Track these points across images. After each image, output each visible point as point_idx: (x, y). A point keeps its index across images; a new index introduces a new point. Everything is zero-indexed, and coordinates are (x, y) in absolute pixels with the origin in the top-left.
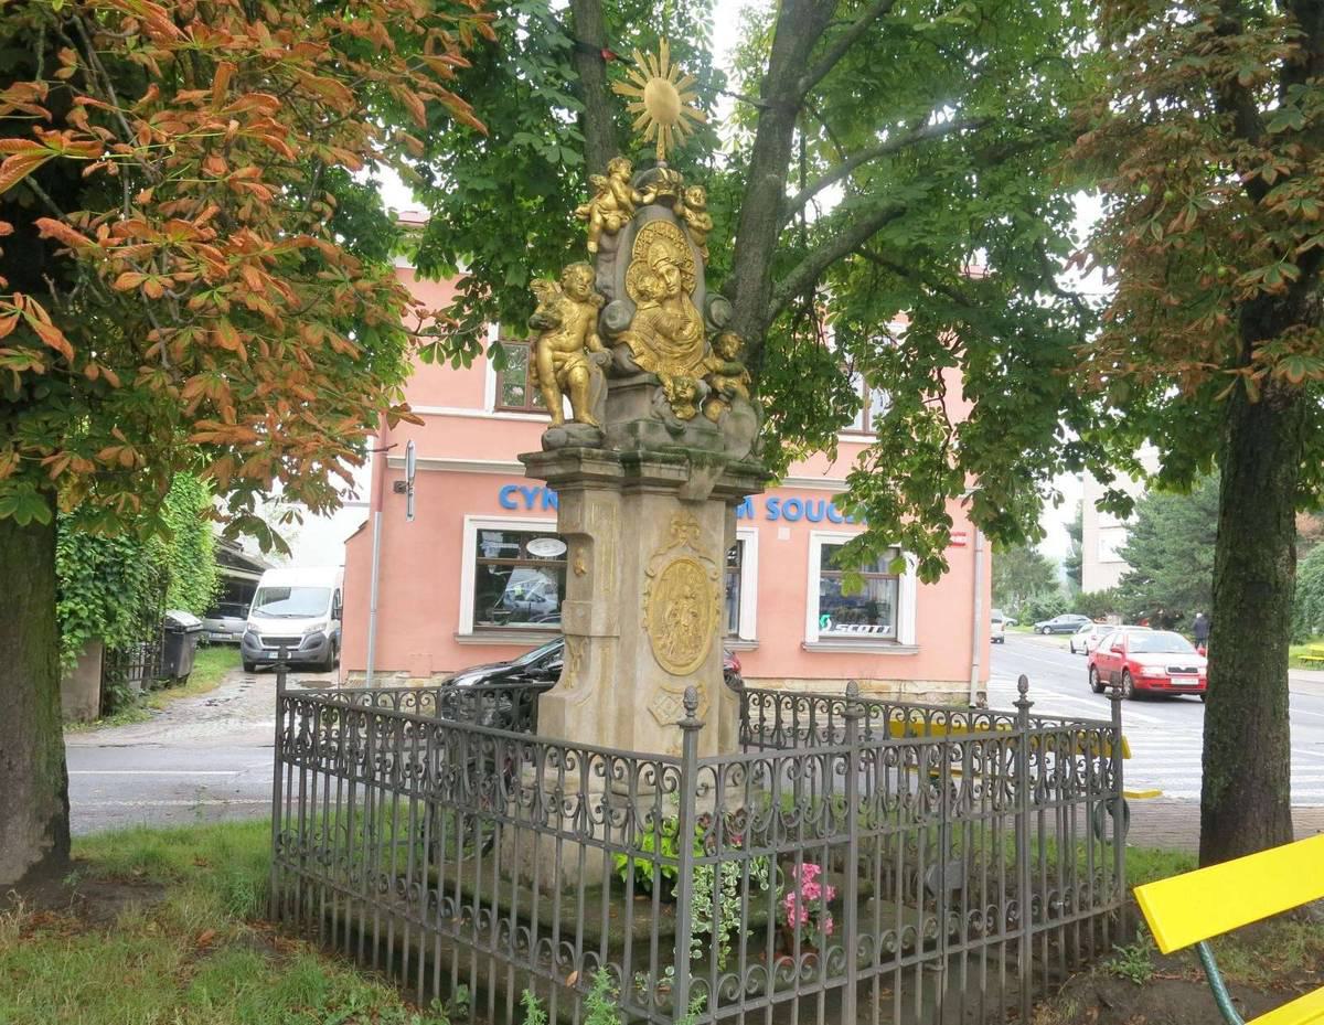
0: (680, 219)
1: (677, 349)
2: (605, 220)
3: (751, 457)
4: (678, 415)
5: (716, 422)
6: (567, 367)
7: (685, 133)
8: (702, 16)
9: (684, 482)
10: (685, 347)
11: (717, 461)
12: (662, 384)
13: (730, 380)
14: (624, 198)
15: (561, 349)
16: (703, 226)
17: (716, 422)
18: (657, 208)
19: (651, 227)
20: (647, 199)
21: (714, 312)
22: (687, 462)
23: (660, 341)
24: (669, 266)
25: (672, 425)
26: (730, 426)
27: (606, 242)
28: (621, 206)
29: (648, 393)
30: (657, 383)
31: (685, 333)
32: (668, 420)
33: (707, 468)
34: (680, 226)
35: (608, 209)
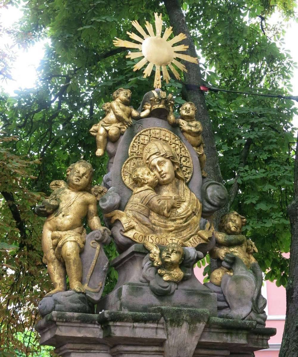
0: (175, 127)
1: (170, 223)
2: (107, 131)
3: (253, 315)
4: (166, 278)
5: (219, 286)
6: (60, 244)
7: (179, 70)
8: (285, 83)
9: (165, 340)
10: (178, 221)
11: (195, 318)
12: (149, 252)
13: (232, 250)
14: (120, 113)
15: (58, 229)
16: (193, 129)
17: (219, 286)
18: (154, 120)
19: (147, 133)
20: (143, 114)
21: (209, 194)
22: (162, 320)
23: (155, 218)
24: (161, 159)
25: (157, 287)
26: (231, 288)
27: (110, 147)
28: (119, 119)
29: (138, 260)
30: (145, 251)
31: (179, 211)
32: (152, 283)
33: (185, 325)
34: (175, 133)
35: (110, 123)
